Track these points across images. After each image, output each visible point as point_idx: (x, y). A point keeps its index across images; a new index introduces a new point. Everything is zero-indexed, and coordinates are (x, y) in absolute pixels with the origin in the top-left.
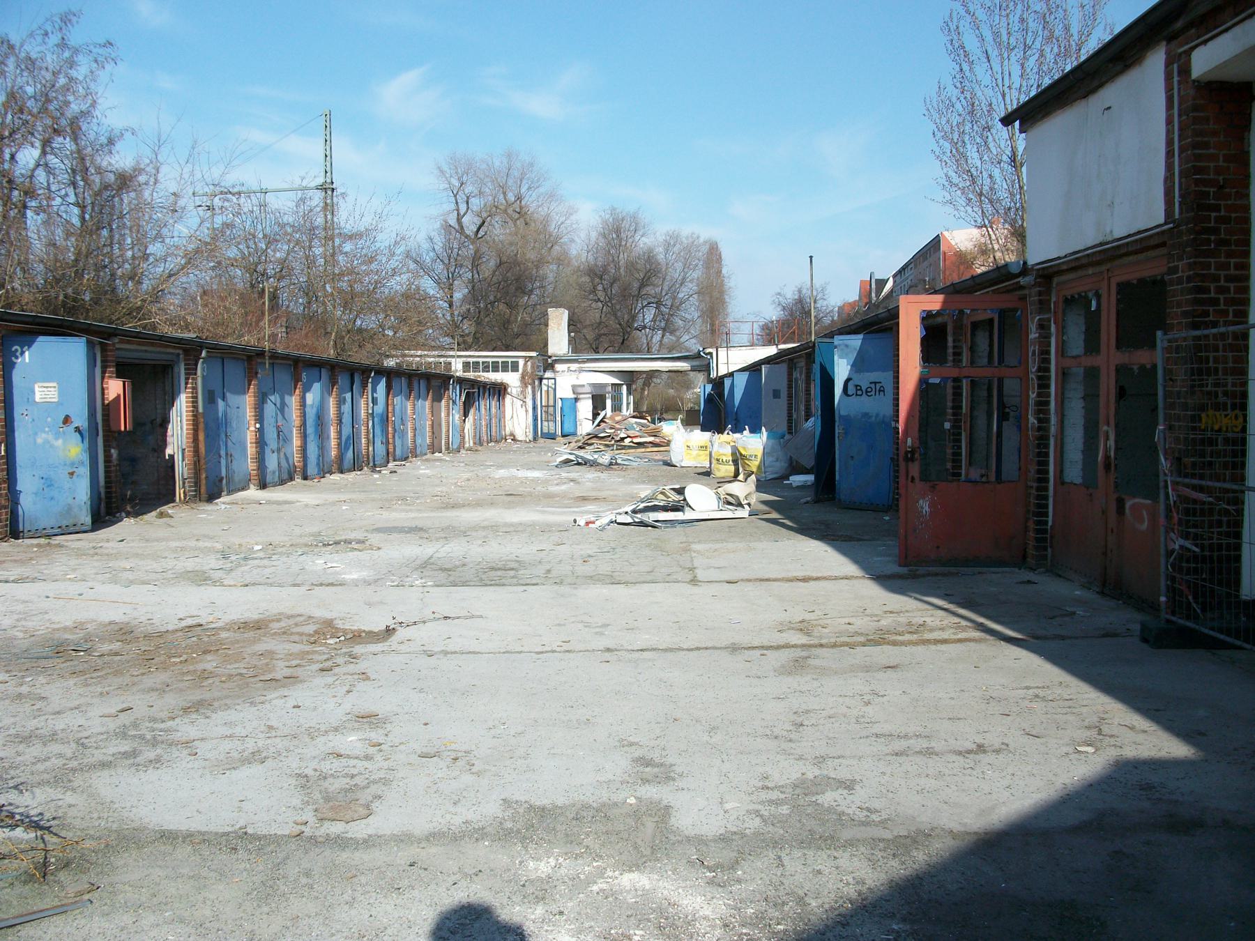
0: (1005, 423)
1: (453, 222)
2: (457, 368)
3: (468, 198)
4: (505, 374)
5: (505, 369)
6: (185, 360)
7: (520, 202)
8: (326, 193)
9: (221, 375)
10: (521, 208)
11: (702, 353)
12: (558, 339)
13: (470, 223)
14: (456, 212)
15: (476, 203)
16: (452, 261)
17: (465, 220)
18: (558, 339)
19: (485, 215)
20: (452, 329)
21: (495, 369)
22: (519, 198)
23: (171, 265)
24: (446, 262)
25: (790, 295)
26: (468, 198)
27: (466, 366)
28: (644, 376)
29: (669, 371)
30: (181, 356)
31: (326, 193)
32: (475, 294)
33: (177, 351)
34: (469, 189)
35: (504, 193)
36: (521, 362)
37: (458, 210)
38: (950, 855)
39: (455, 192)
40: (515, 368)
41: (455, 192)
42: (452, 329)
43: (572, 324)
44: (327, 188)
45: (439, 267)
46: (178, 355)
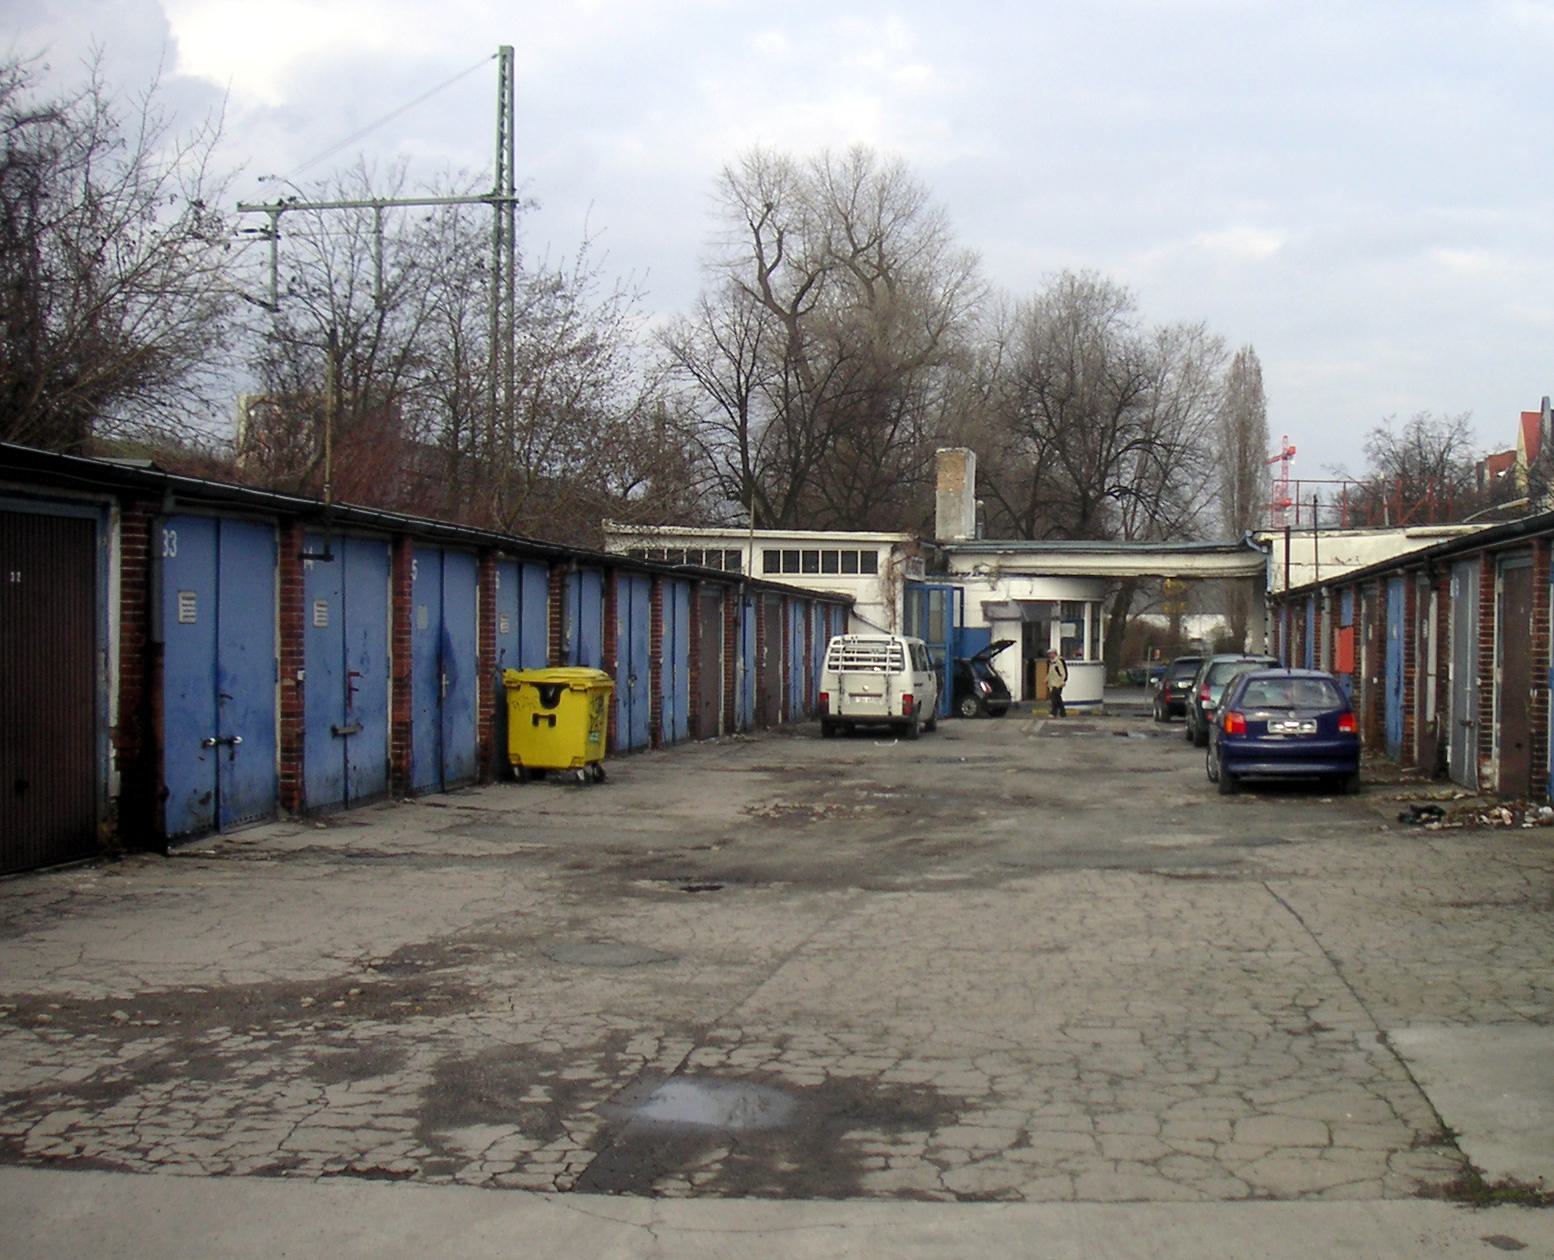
0: (748, 609)
1: (751, 279)
2: (753, 566)
3: (781, 234)
4: (119, 563)
5: (849, 568)
6: (124, 519)
7: (880, 245)
8: (500, 209)
9: (211, 579)
10: (882, 257)
11: (1250, 544)
12: (958, 520)
13: (781, 281)
14: (756, 262)
15: (796, 247)
16: (746, 352)
17: (777, 277)
18: (958, 520)
19: (810, 269)
20: (747, 490)
21: (830, 568)
22: (878, 238)
23: (229, 1055)
24: (735, 352)
25: (1400, 435)
26: (781, 234)
27: (771, 561)
28: (1119, 586)
29: (1180, 578)
30: (114, 510)
31: (500, 209)
32: (787, 422)
33: (103, 498)
34: (783, 217)
35: (849, 228)
36: (883, 556)
37: (760, 257)
38: (161, 558)
39: (756, 225)
40: (869, 564)
41: (756, 225)
42: (747, 490)
43: (985, 482)
44: (503, 201)
45: (723, 365)
46: (105, 507)
